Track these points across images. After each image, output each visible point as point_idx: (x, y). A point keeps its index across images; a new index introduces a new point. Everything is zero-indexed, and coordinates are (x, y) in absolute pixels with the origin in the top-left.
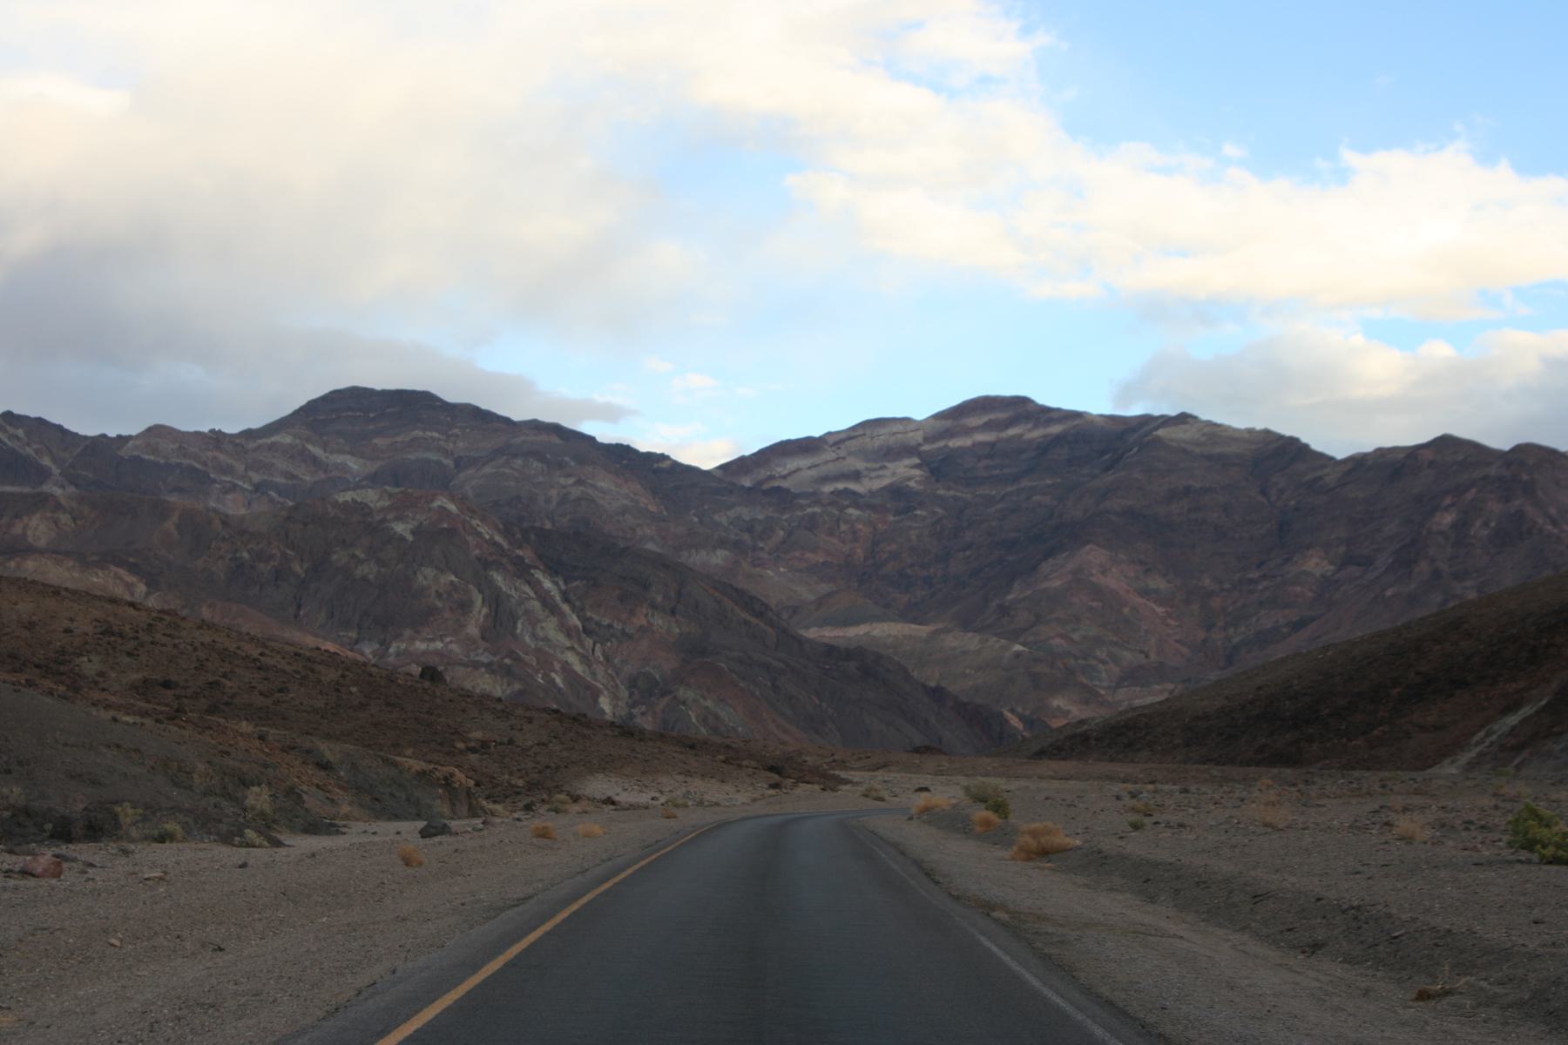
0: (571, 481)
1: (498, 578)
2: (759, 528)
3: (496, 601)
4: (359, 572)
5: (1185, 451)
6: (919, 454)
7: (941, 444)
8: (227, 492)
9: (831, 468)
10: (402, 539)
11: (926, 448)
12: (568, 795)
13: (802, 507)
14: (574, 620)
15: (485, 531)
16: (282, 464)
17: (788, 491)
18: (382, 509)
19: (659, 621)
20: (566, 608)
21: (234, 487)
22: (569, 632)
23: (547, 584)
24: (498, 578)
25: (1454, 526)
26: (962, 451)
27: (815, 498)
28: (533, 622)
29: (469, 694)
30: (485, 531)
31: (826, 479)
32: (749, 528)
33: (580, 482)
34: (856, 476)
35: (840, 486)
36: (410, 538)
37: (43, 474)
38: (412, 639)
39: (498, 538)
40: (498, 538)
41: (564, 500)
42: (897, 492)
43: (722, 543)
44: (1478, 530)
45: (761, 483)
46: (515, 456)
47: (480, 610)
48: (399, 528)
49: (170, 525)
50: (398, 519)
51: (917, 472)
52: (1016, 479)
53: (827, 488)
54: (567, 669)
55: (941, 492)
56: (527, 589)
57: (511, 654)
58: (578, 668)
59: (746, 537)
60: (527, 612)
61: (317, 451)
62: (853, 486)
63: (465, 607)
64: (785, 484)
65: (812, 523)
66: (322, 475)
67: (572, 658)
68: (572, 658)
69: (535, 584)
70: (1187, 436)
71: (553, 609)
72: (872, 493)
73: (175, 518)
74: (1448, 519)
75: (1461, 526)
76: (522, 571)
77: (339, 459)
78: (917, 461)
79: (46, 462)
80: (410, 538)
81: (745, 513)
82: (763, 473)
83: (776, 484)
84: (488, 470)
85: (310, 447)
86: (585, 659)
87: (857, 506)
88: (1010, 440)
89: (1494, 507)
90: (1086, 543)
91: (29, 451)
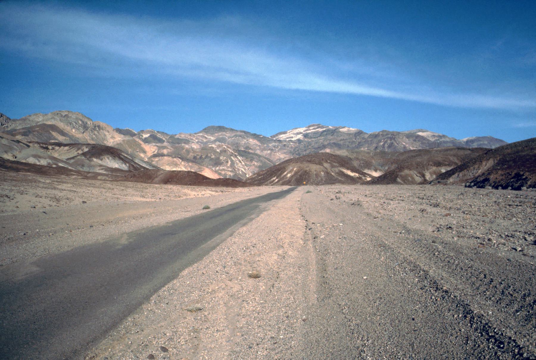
0: (246, 140)
1: (232, 157)
2: (276, 147)
3: (232, 161)
4: (212, 157)
5: (344, 133)
6: (303, 134)
7: (306, 132)
8: (192, 143)
9: (287, 137)
10: (218, 152)
11: (304, 133)
12: (529, 256)
13: (283, 143)
14: (243, 163)
15: (230, 150)
16: (201, 138)
17: (281, 140)
18: (215, 148)
19: (256, 163)
20: (242, 162)
21: (193, 142)
22: (243, 165)
23: (239, 158)
24: (232, 157)
25: (383, 145)
26: (309, 133)
27: (285, 141)
28: (237, 164)
29: (185, 194)
30: (230, 150)
31: (287, 138)
32: (275, 147)
33: (247, 140)
34: (292, 137)
35: (290, 139)
36: (219, 152)
37: (164, 141)
38: (220, 167)
39: (232, 152)
40: (232, 152)
41: (245, 143)
42: (299, 141)
43: (269, 150)
44: (386, 145)
45: (277, 139)
46: (237, 136)
47: (230, 163)
48: (218, 150)
49: (184, 151)
50: (218, 149)
51: (302, 137)
52: (317, 137)
53: (288, 140)
54: (242, 171)
55: (306, 140)
56: (236, 159)
57: (234, 169)
58: (244, 171)
59: (274, 148)
60: (237, 163)
61: (206, 136)
62: (292, 139)
63: (227, 162)
64: (281, 139)
65: (285, 145)
66: (207, 140)
67: (243, 170)
68: (243, 170)
69: (238, 158)
70: (345, 130)
71: (241, 162)
72: (295, 140)
73: (185, 150)
74: (382, 144)
75: (384, 145)
76: (236, 156)
77: (209, 137)
78: (302, 135)
79: (164, 139)
80: (219, 152)
81: (274, 144)
82: (277, 137)
83: (279, 139)
84: (233, 139)
85: (205, 135)
86: (245, 169)
87: (292, 142)
88: (317, 131)
89: (389, 142)
90: (326, 148)
91: (161, 137)
